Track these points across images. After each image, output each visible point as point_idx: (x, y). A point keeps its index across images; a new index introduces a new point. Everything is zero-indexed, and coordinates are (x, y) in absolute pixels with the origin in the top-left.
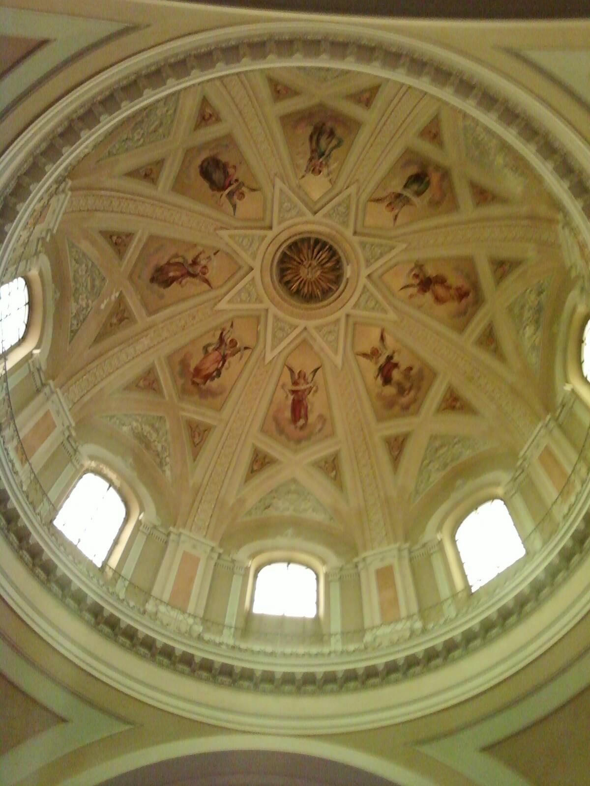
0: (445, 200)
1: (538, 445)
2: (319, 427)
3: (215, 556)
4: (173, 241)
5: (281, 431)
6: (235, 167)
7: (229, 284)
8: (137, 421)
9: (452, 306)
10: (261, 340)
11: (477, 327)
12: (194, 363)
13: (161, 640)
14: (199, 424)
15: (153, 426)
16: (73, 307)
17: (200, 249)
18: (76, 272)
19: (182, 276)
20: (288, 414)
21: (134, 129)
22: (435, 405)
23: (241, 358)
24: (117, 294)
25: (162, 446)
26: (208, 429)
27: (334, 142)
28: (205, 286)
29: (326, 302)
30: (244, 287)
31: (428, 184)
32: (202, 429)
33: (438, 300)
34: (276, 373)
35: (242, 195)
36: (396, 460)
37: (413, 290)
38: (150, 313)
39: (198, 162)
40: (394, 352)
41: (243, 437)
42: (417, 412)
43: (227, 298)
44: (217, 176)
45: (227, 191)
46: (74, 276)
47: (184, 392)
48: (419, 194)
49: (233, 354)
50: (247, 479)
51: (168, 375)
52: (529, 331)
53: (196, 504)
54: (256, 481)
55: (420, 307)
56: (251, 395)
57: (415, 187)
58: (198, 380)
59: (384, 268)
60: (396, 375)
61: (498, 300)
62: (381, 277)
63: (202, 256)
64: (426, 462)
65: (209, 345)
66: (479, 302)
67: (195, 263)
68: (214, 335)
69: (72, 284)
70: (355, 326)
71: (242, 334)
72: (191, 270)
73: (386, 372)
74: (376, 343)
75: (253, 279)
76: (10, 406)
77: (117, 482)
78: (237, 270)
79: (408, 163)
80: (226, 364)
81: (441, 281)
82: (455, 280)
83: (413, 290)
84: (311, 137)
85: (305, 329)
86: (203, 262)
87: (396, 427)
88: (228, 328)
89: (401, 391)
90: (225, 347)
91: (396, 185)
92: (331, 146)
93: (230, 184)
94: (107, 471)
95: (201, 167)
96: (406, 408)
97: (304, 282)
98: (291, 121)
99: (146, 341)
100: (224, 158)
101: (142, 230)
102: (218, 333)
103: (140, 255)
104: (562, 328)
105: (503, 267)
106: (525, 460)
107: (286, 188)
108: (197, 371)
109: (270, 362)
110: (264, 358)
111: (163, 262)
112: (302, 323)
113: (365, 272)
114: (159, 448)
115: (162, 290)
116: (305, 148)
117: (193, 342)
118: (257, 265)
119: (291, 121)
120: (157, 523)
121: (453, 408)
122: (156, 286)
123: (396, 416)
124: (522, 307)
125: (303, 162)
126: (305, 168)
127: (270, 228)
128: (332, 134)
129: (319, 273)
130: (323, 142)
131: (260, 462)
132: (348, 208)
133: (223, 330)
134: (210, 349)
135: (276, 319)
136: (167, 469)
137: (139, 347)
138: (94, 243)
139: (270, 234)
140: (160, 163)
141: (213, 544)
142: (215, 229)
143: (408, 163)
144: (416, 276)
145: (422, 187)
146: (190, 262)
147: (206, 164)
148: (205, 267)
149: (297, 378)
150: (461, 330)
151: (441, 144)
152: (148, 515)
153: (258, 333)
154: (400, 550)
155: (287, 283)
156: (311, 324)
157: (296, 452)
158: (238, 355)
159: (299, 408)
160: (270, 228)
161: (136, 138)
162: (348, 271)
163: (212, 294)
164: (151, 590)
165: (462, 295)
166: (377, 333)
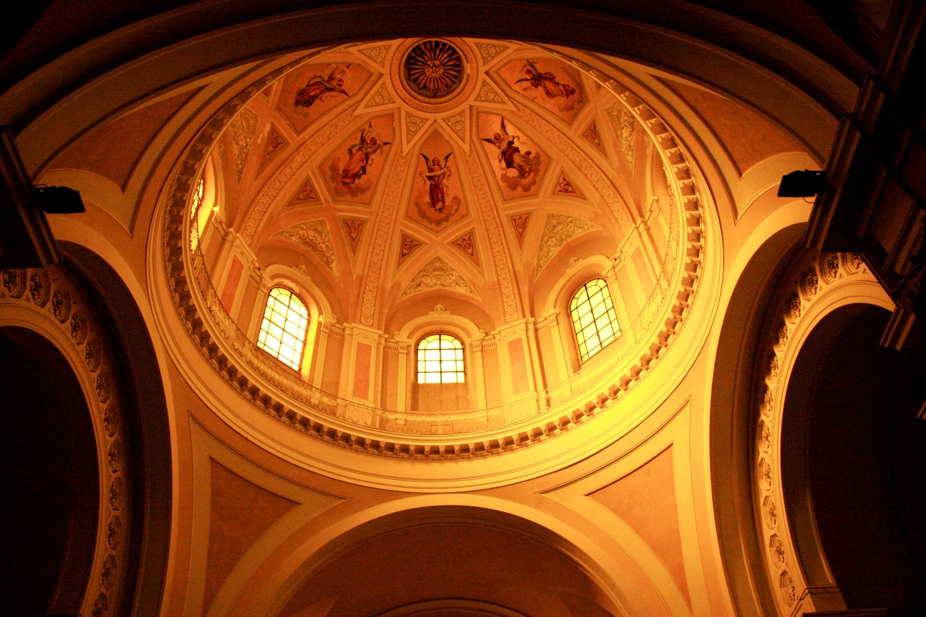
1: (632, 244)
2: (455, 207)
3: (383, 342)
5: (423, 215)
8: (303, 229)
9: (562, 100)
10: (397, 136)
12: (342, 166)
13: (355, 434)
14: (353, 221)
16: (235, 148)
17: (334, 66)
19: (322, 92)
20: (427, 199)
22: (550, 190)
25: (327, 246)
26: (362, 223)
28: (343, 96)
30: (378, 92)
32: (356, 223)
33: (548, 93)
34: (413, 166)
36: (520, 236)
37: (527, 84)
38: (299, 133)
42: (536, 195)
49: (374, 152)
50: (399, 264)
51: (322, 183)
53: (361, 295)
56: (395, 185)
58: (347, 181)
60: (517, 159)
62: (497, 72)
64: (545, 238)
65: (353, 147)
66: (583, 100)
67: (331, 78)
71: (380, 132)
72: (328, 85)
73: (509, 155)
74: (497, 129)
75: (384, 83)
76: (206, 272)
80: (370, 162)
81: (551, 78)
85: (435, 121)
89: (522, 173)
90: (367, 146)
99: (298, 158)
109: (408, 154)
110: (401, 152)
111: (303, 86)
112: (431, 116)
114: (325, 249)
115: (306, 110)
117: (339, 147)
118: (386, 71)
120: (334, 321)
121: (567, 191)
122: (300, 107)
129: (442, 70)
131: (409, 246)
133: (364, 130)
134: (354, 150)
136: (334, 265)
137: (295, 165)
141: (380, 332)
144: (529, 72)
146: (327, 79)
148: (341, 80)
149: (431, 164)
152: (328, 318)
153: (394, 129)
154: (527, 324)
155: (415, 80)
156: (439, 116)
157: (437, 232)
158: (379, 151)
162: (468, 69)
164: (337, 391)
166: (497, 121)
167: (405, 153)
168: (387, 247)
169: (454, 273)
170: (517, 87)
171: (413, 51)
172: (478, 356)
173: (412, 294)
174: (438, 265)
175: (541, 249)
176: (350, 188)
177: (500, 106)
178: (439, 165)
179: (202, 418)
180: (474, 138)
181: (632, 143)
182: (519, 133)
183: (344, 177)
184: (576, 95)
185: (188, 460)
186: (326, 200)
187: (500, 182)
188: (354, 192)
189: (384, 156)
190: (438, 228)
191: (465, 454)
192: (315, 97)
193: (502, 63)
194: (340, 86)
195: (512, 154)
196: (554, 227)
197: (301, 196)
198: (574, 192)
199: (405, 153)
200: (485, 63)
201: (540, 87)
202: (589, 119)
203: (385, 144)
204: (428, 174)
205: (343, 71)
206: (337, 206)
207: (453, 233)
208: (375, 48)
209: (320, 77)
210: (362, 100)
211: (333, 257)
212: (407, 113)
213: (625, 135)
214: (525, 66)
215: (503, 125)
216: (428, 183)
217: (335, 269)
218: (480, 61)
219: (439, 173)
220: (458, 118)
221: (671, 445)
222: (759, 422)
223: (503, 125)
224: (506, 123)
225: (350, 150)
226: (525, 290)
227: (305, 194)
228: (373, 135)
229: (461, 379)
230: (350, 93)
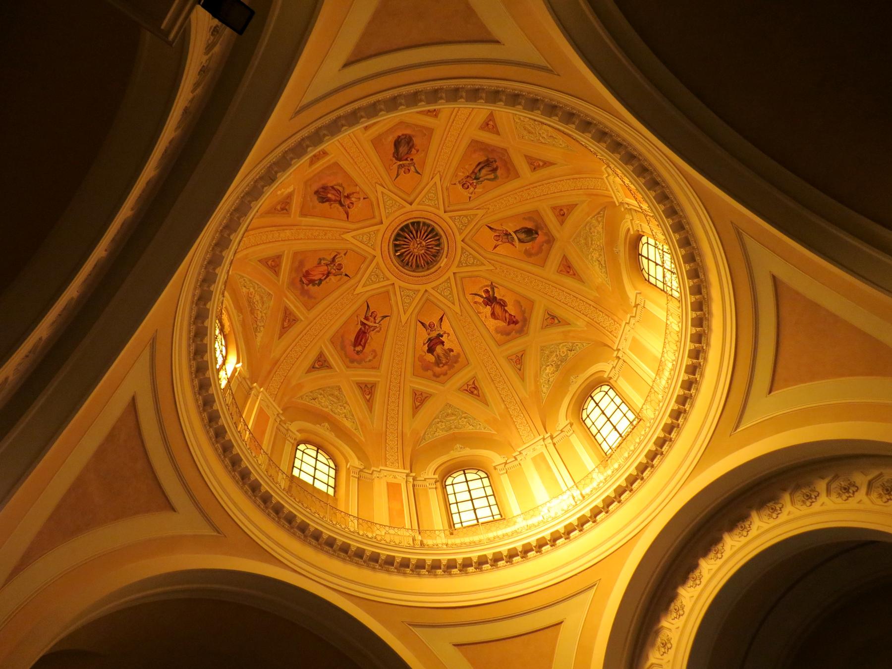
0: (539, 256)
2: (370, 358)
4: (346, 175)
5: (343, 348)
6: (418, 151)
8: (254, 288)
9: (501, 324)
10: (359, 276)
19: (335, 201)
20: (352, 337)
27: (492, 176)
30: (369, 233)
31: (534, 239)
33: (493, 315)
34: (355, 307)
36: (416, 409)
41: (305, 332)
42: (443, 383)
44: (403, 149)
47: (292, 283)
48: (520, 241)
50: (309, 371)
52: (549, 370)
57: (523, 236)
58: (304, 279)
60: (439, 349)
61: (536, 337)
62: (462, 278)
63: (355, 195)
65: (324, 259)
66: (522, 332)
67: (348, 197)
70: (428, 303)
73: (433, 344)
75: (378, 230)
79: (530, 219)
80: (327, 280)
81: (503, 304)
82: (511, 309)
83: (481, 300)
84: (479, 164)
86: (353, 199)
87: (424, 385)
88: (342, 254)
89: (438, 362)
92: (489, 177)
93: (406, 160)
95: (399, 137)
96: (436, 376)
97: (411, 253)
99: (288, 233)
100: (417, 141)
106: (520, 453)
108: (307, 273)
111: (330, 184)
113: (454, 269)
116: (470, 168)
117: (315, 251)
118: (386, 222)
121: (472, 393)
122: (315, 198)
125: (461, 175)
127: (411, 204)
128: (495, 170)
130: (484, 172)
131: (321, 363)
135: (378, 266)
136: (260, 335)
143: (530, 219)
144: (487, 291)
145: (529, 238)
151: (562, 223)
154: (407, 475)
157: (348, 367)
158: (339, 277)
159: (361, 338)
160: (411, 204)
162: (443, 262)
165: (513, 321)
168: (306, 352)
169: (347, 407)
170: (470, 297)
171: (413, 224)
172: (354, 483)
174: (336, 393)
175: (430, 426)
176: (303, 288)
177: (449, 304)
180: (414, 316)
181: (551, 380)
182: (451, 332)
183: (304, 276)
185: (125, 378)
187: (417, 359)
188: (304, 293)
190: (350, 365)
191: (342, 554)
192: (329, 200)
193: (470, 274)
195: (437, 344)
196: (448, 415)
197: (269, 263)
203: (346, 275)
206: (288, 294)
210: (355, 230)
211: (262, 329)
212: (377, 264)
213: (548, 371)
216: (360, 326)
217: (259, 339)
218: (456, 262)
221: (562, 623)
222: (655, 628)
224: (445, 318)
226: (408, 450)
227: (273, 264)
229: (331, 492)
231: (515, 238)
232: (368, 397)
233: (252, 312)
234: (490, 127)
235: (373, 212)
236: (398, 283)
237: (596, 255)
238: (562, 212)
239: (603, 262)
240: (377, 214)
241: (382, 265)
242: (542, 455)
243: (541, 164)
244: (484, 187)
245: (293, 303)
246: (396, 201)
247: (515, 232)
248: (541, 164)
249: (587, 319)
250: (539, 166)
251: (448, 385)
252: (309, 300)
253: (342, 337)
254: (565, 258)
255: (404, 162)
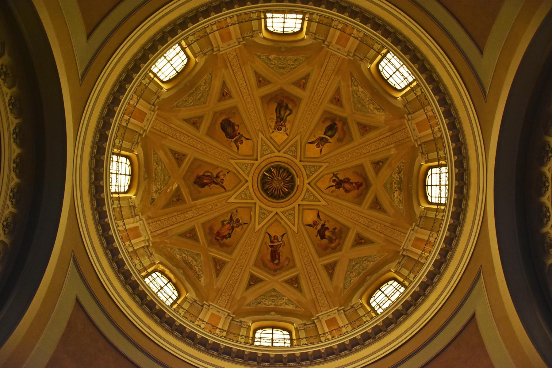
0: (345, 137)
2: (287, 263)
5: (265, 266)
6: (238, 126)
7: (235, 189)
8: (185, 254)
9: (354, 193)
11: (369, 199)
12: (216, 229)
15: (193, 258)
17: (220, 169)
18: (156, 169)
19: (211, 183)
20: (269, 257)
21: (189, 96)
22: (350, 244)
23: (242, 228)
24: (176, 186)
25: (199, 269)
27: (288, 112)
28: (223, 190)
29: (286, 199)
33: (347, 191)
35: (242, 142)
37: (334, 188)
38: (194, 200)
39: (220, 121)
40: (325, 222)
42: (340, 250)
43: (235, 196)
44: (229, 130)
45: (234, 139)
46: (155, 172)
47: (211, 244)
48: (331, 136)
54: (252, 289)
55: (337, 197)
56: (247, 249)
57: (330, 133)
58: (217, 238)
59: (317, 179)
60: (327, 233)
61: (378, 183)
63: (221, 174)
65: (225, 221)
67: (217, 177)
68: (227, 216)
69: (154, 175)
71: (242, 216)
72: (215, 180)
73: (321, 234)
74: (316, 219)
77: (174, 280)
78: (240, 182)
81: (347, 181)
83: (334, 188)
86: (222, 177)
89: (331, 241)
90: (233, 223)
91: (320, 134)
93: (236, 135)
94: (167, 272)
95: (221, 123)
98: (267, 100)
99: (190, 214)
101: (191, 155)
102: (229, 215)
103: (189, 167)
104: (414, 183)
105: (378, 165)
107: (264, 138)
108: (218, 233)
109: (258, 231)
112: (275, 211)
114: (197, 270)
115: (200, 189)
117: (215, 219)
119: (267, 100)
121: (361, 243)
122: (196, 186)
123: (330, 253)
124: (391, 183)
126: (273, 127)
128: (287, 107)
130: (282, 113)
131: (254, 281)
132: (296, 148)
133: (232, 213)
134: (225, 223)
136: (202, 280)
138: (166, 154)
139: (257, 163)
140: (201, 118)
142: (228, 159)
144: (334, 181)
147: (224, 122)
148: (223, 179)
150: (360, 204)
151: (341, 105)
153: (251, 216)
157: (274, 275)
158: (241, 227)
159: (275, 254)
161: (190, 101)
162: (298, 182)
163: (227, 194)
165: (359, 185)
167: (256, 230)
173: (254, 307)
174: (274, 293)
178: (277, 240)
179: (78, 259)
181: (401, 199)
183: (217, 236)
184: (364, 186)
186: (203, 243)
188: (223, 245)
189: (243, 231)
194: (222, 183)
198: (366, 242)
199: (256, 230)
200: (308, 178)
201: (341, 189)
202: (373, 196)
203: (245, 224)
204: (270, 244)
205: (225, 174)
206: (212, 250)
207: (285, 276)
208: (245, 164)
209: (211, 173)
211: (202, 275)
212: (260, 206)
214: (332, 177)
215: (318, 216)
216: (270, 249)
219: (276, 244)
220: (291, 212)
221: (474, 315)
223: (318, 216)
224: (320, 214)
225: (223, 222)
228: (238, 217)
230: (227, 189)
231: (327, 137)
232: (296, 286)
233: (191, 268)
234: (262, 81)
235: (239, 178)
236: (279, 211)
237: (371, 107)
238: (337, 99)
239: (378, 107)
240: (241, 178)
241: (263, 206)
242: (417, 239)
243: (304, 81)
244: (289, 122)
245: (215, 253)
246: (247, 164)
247: (324, 134)
248: (304, 81)
249: (393, 145)
250: (304, 83)
251: (344, 250)
252: (229, 249)
253: (262, 260)
254: (359, 124)
255: (236, 138)
